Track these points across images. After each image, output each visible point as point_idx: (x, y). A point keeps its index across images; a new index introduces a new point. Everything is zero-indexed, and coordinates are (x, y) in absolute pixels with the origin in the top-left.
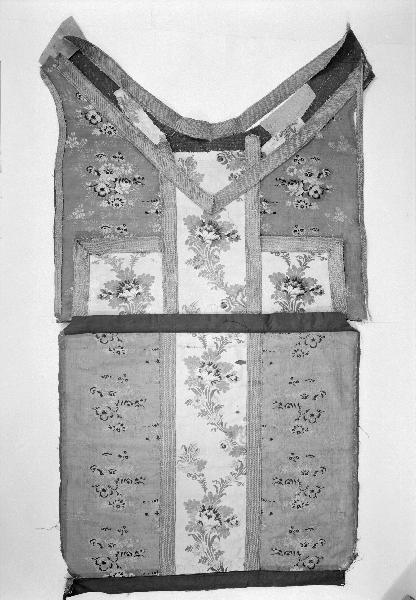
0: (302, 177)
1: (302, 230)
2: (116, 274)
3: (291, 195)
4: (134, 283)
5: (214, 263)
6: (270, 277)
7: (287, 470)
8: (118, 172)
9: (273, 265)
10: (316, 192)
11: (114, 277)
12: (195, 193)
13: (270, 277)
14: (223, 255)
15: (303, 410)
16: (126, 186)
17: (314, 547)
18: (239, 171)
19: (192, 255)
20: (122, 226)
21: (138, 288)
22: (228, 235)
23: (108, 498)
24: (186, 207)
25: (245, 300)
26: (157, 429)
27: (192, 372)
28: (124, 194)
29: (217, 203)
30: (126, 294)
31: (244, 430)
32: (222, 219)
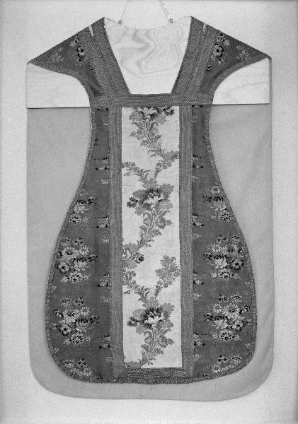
0: (226, 313)
1: (225, 360)
3: (218, 328)
8: (76, 253)
10: (238, 326)
20: (79, 300)
22: (164, 110)
26: (105, 162)
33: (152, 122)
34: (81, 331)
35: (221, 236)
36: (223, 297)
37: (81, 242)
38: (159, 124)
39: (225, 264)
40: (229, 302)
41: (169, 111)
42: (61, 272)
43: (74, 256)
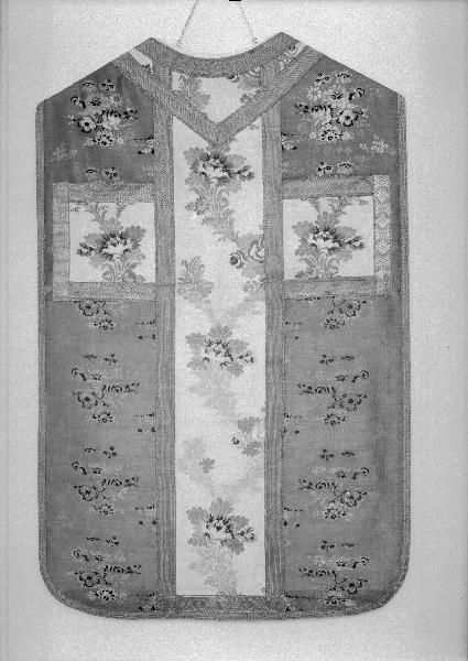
2: (99, 225)
4: (121, 238)
5: (222, 208)
6: (294, 227)
7: (319, 471)
9: (298, 211)
10: (348, 118)
11: (96, 229)
12: (198, 122)
13: (294, 227)
14: (232, 197)
15: (339, 579)
16: (114, 121)
17: (354, 567)
18: (253, 91)
19: (193, 197)
20: (111, 171)
21: (126, 243)
22: (239, 172)
23: (94, 502)
24: (184, 138)
25: (262, 253)
27: (197, 353)
28: (113, 131)
29: (229, 128)
30: (111, 250)
31: (263, 422)
32: (231, 152)
33: (219, 189)
34: (110, 129)
35: (322, 164)
36: (323, 77)
37: (115, 175)
38: (231, 192)
39: (329, 118)
40: (332, 83)
41: (246, 174)
42: (83, 131)
43: (105, 107)
